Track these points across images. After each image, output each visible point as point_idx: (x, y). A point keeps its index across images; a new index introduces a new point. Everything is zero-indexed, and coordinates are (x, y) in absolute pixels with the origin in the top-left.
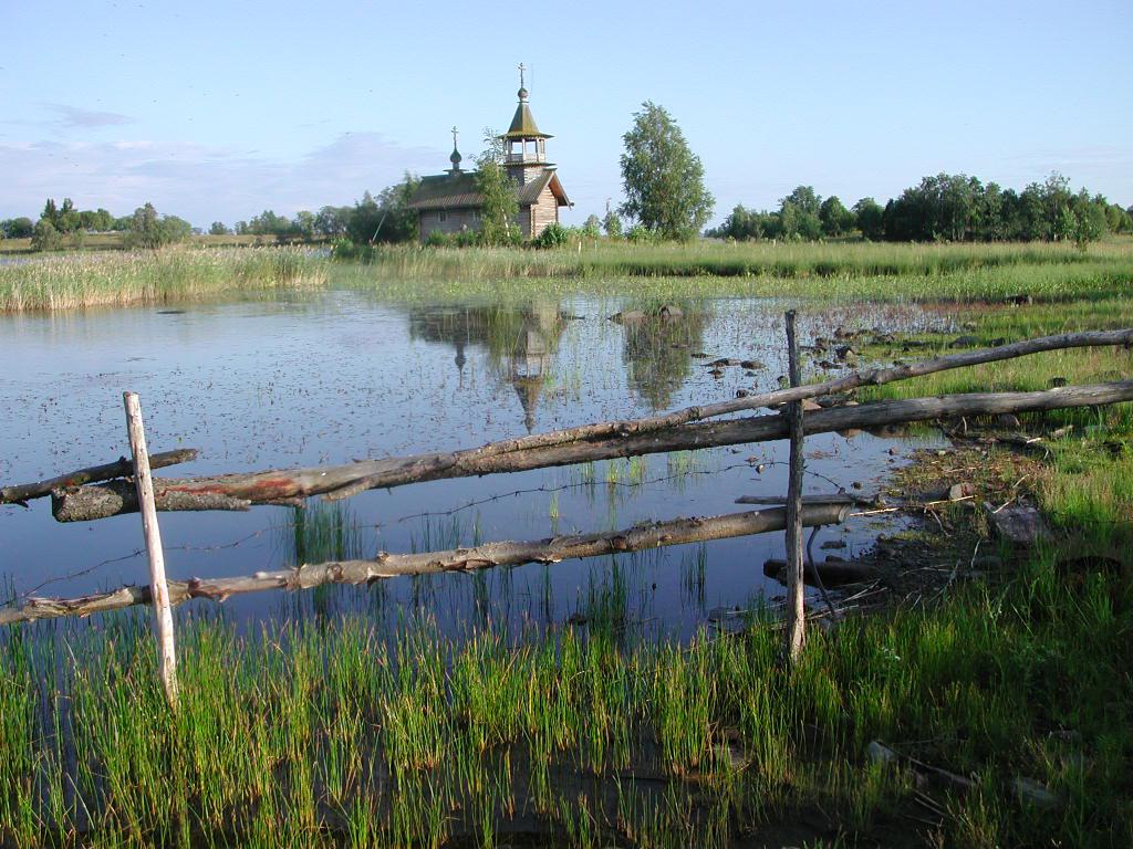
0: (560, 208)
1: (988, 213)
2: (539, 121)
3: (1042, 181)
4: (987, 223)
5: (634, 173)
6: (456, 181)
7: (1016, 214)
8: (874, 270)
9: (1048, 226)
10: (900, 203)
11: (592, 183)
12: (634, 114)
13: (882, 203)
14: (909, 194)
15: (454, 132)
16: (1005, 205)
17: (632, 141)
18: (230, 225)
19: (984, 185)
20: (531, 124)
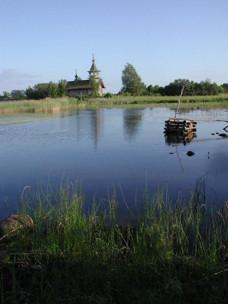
0: (103, 89)
1: (191, 88)
2: (98, 67)
3: (204, 80)
4: (191, 91)
5: (125, 80)
6: (78, 82)
7: (198, 89)
8: (190, 101)
9: (206, 91)
10: (168, 86)
11: (113, 84)
12: (125, 66)
13: (164, 86)
14: (171, 84)
15: (76, 70)
16: (196, 86)
17: (124, 72)
18: (113, 94)
19: (190, 81)
20: (96, 68)
